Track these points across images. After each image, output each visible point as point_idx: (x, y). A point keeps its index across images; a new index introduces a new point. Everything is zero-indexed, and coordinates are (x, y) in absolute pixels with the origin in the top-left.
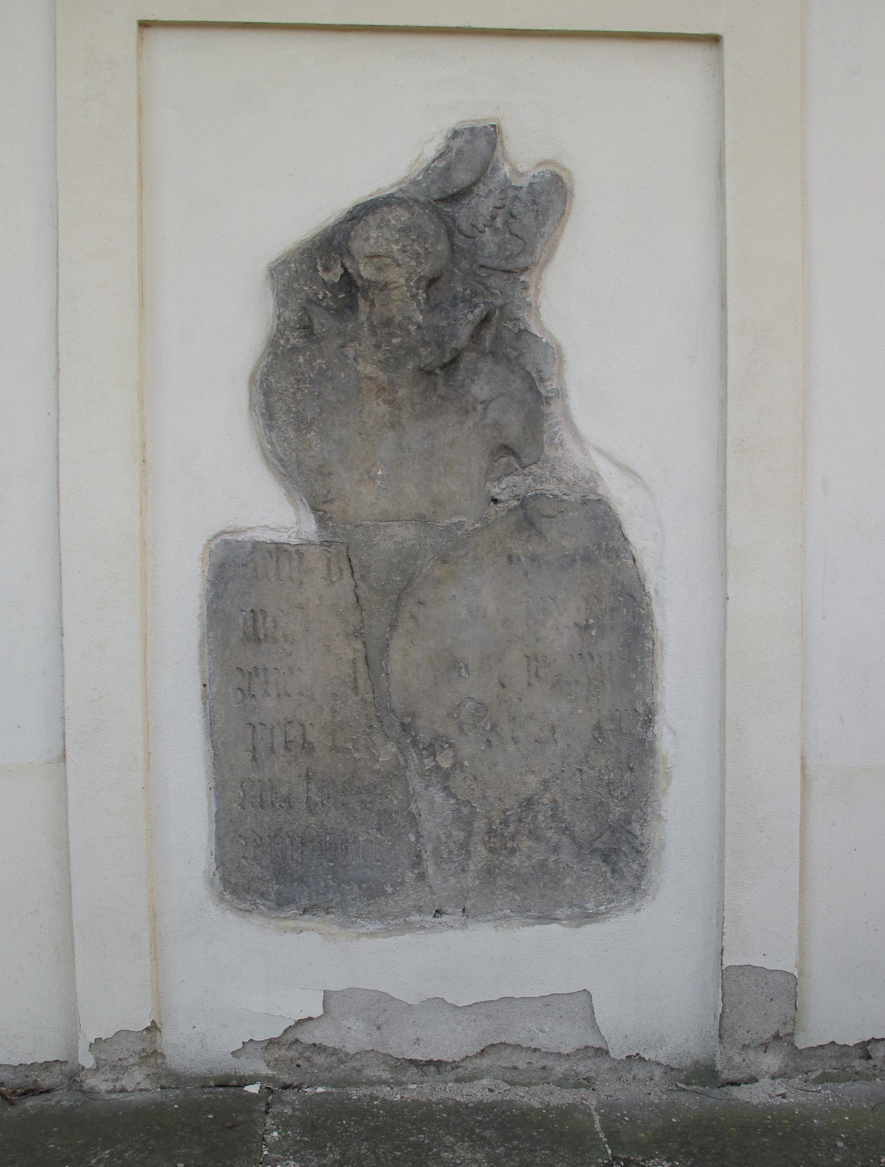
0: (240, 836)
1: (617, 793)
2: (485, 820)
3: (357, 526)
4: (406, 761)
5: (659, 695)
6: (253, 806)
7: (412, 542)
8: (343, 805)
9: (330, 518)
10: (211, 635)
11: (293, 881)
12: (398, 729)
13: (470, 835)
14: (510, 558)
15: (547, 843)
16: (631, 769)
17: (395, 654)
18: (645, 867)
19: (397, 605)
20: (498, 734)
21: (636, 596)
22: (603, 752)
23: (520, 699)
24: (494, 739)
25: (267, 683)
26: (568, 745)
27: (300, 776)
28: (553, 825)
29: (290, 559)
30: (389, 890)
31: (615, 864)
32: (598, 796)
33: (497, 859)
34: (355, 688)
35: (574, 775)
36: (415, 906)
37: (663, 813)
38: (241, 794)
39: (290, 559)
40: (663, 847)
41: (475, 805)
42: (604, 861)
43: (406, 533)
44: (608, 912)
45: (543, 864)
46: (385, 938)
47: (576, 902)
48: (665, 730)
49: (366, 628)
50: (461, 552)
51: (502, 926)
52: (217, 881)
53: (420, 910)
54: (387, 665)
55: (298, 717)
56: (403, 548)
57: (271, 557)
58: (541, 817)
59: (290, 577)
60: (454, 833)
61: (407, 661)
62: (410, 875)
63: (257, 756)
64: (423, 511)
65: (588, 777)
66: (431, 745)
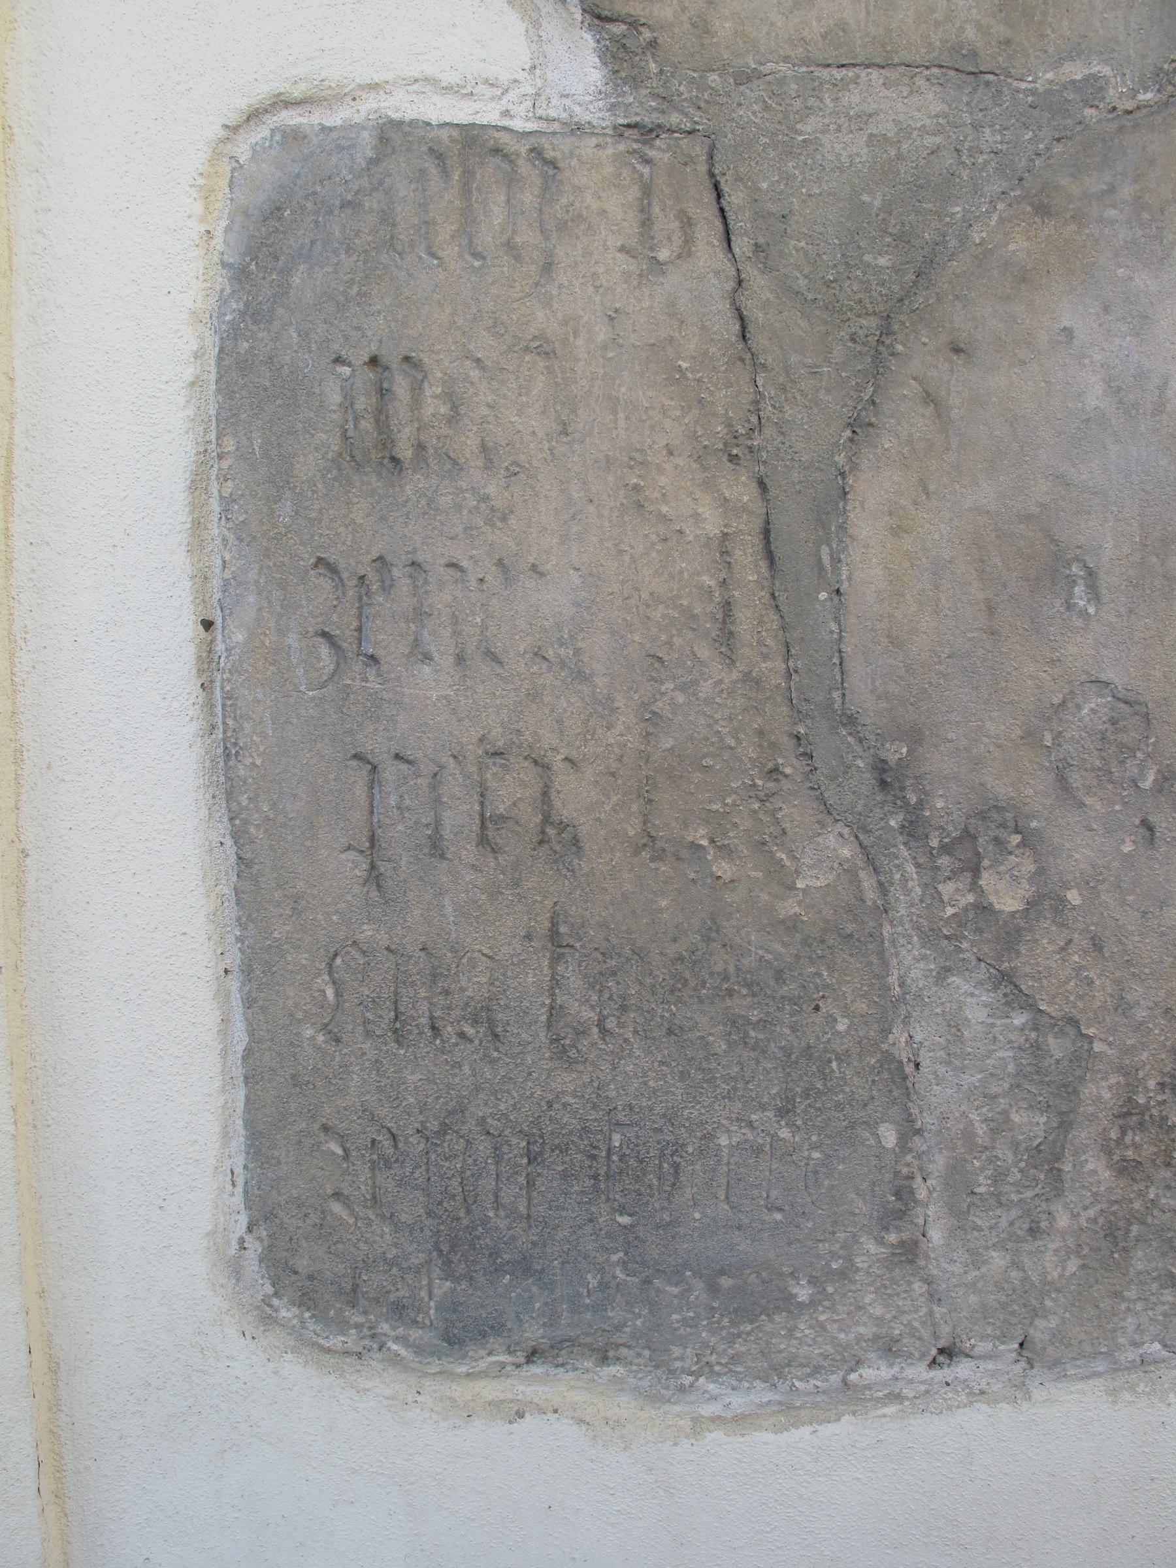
0: (325, 1129)
3: (745, 78)
4: (883, 889)
6: (368, 1034)
7: (931, 141)
8: (670, 1032)
9: (653, 44)
10: (230, 445)
11: (498, 1270)
12: (863, 779)
13: (1065, 1124)
17: (866, 526)
19: (879, 354)
25: (420, 614)
27: (529, 937)
29: (512, 181)
30: (803, 1293)
34: (726, 638)
36: (876, 1338)
38: (330, 993)
39: (512, 181)
41: (1091, 1031)
43: (913, 109)
46: (778, 1429)
49: (769, 431)
50: (1095, 183)
51: (1132, 1389)
52: (252, 1264)
53: (890, 1349)
54: (836, 561)
55: (528, 737)
56: (900, 157)
57: (445, 173)
59: (509, 245)
60: (1016, 1118)
61: (900, 551)
62: (872, 1247)
63: (383, 867)
64: (970, 33)
66: (968, 836)
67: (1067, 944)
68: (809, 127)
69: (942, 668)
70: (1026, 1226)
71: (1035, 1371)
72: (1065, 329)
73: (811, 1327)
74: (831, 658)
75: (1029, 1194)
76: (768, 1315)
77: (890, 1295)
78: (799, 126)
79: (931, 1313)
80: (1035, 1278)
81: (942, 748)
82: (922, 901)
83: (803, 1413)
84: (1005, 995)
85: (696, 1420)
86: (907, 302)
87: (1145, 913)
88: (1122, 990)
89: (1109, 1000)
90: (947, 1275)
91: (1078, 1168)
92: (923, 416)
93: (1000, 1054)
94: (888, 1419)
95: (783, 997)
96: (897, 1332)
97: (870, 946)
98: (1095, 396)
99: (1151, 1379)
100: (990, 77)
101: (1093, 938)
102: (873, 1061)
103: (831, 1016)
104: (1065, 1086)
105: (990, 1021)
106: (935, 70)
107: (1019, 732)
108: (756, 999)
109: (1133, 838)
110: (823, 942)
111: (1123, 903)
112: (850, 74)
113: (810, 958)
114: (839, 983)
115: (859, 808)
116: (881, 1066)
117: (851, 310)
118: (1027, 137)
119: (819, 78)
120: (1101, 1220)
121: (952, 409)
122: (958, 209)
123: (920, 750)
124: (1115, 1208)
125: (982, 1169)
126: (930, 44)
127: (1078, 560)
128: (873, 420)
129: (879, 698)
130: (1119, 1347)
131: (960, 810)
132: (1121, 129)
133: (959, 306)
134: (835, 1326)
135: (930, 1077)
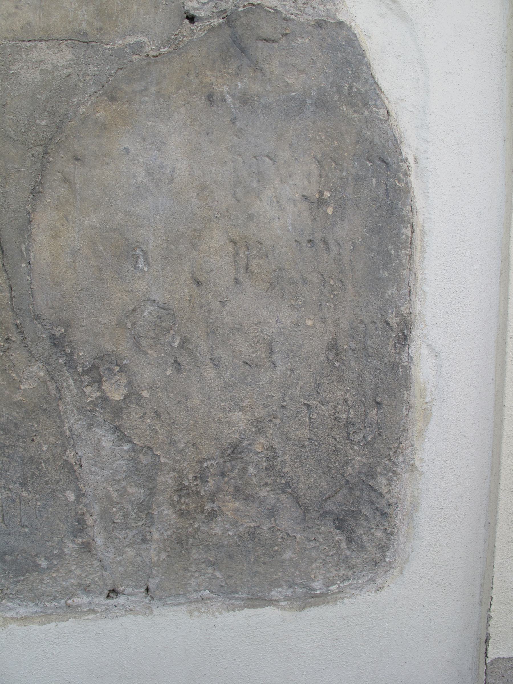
1: (358, 438)
2: (172, 474)
4: (58, 390)
5: (418, 303)
7: (66, 71)
13: (152, 493)
14: (210, 98)
15: (260, 504)
16: (378, 404)
17: (40, 234)
18: (392, 534)
19: (43, 162)
20: (191, 353)
21: (389, 160)
22: (341, 381)
23: (223, 303)
24: (184, 360)
26: (292, 370)
28: (269, 481)
30: (44, 564)
31: (353, 531)
32: (332, 441)
33: (191, 525)
35: (299, 412)
36: (80, 585)
37: (417, 463)
40: (416, 506)
41: (159, 453)
42: (337, 528)
43: (58, 58)
44: (340, 591)
45: (254, 534)
46: (41, 624)
47: (298, 580)
48: (424, 351)
50: (138, 86)
51: (199, 610)
53: (87, 590)
54: (28, 250)
56: (53, 79)
58: (251, 470)
60: (130, 490)
62: (70, 545)
64: (84, 25)
65: (319, 416)
66: (95, 367)
67: (144, 414)
68: (15, 67)
69: (78, 295)
70: (141, 538)
71: (154, 602)
72: (125, 148)
73: (50, 579)
74: (28, 291)
75: (140, 524)
76: (30, 573)
77: (83, 566)
78: (11, 67)
79: (102, 575)
80: (147, 561)
81: (80, 329)
82: (77, 395)
83: (52, 617)
84: (118, 436)
85: (5, 619)
86: (53, 140)
87: (179, 402)
88: (172, 435)
89: (166, 439)
90: (107, 558)
91: (160, 513)
92: (64, 188)
93: (119, 462)
94: (89, 621)
95: (19, 435)
96: (88, 582)
97: (55, 414)
98: (141, 177)
99: (208, 607)
100: (94, 44)
101: (156, 412)
102: (60, 464)
103: (40, 443)
104: (149, 476)
105: (113, 447)
106: (69, 42)
107: (115, 322)
108: (7, 436)
109: (171, 368)
110: (34, 412)
111: (168, 397)
112: (33, 44)
113: (29, 418)
114: (42, 430)
115: (46, 355)
116: (64, 466)
117: (32, 144)
118: (107, 68)
119: (20, 46)
120: (174, 536)
121: (76, 184)
122: (76, 99)
123: (70, 330)
124: (180, 531)
125: (117, 512)
126: (67, 30)
127: (139, 248)
128: (41, 190)
129: (50, 308)
130: (189, 592)
131: (91, 356)
132: (148, 63)
133: (76, 141)
134: (61, 579)
135: (88, 471)
